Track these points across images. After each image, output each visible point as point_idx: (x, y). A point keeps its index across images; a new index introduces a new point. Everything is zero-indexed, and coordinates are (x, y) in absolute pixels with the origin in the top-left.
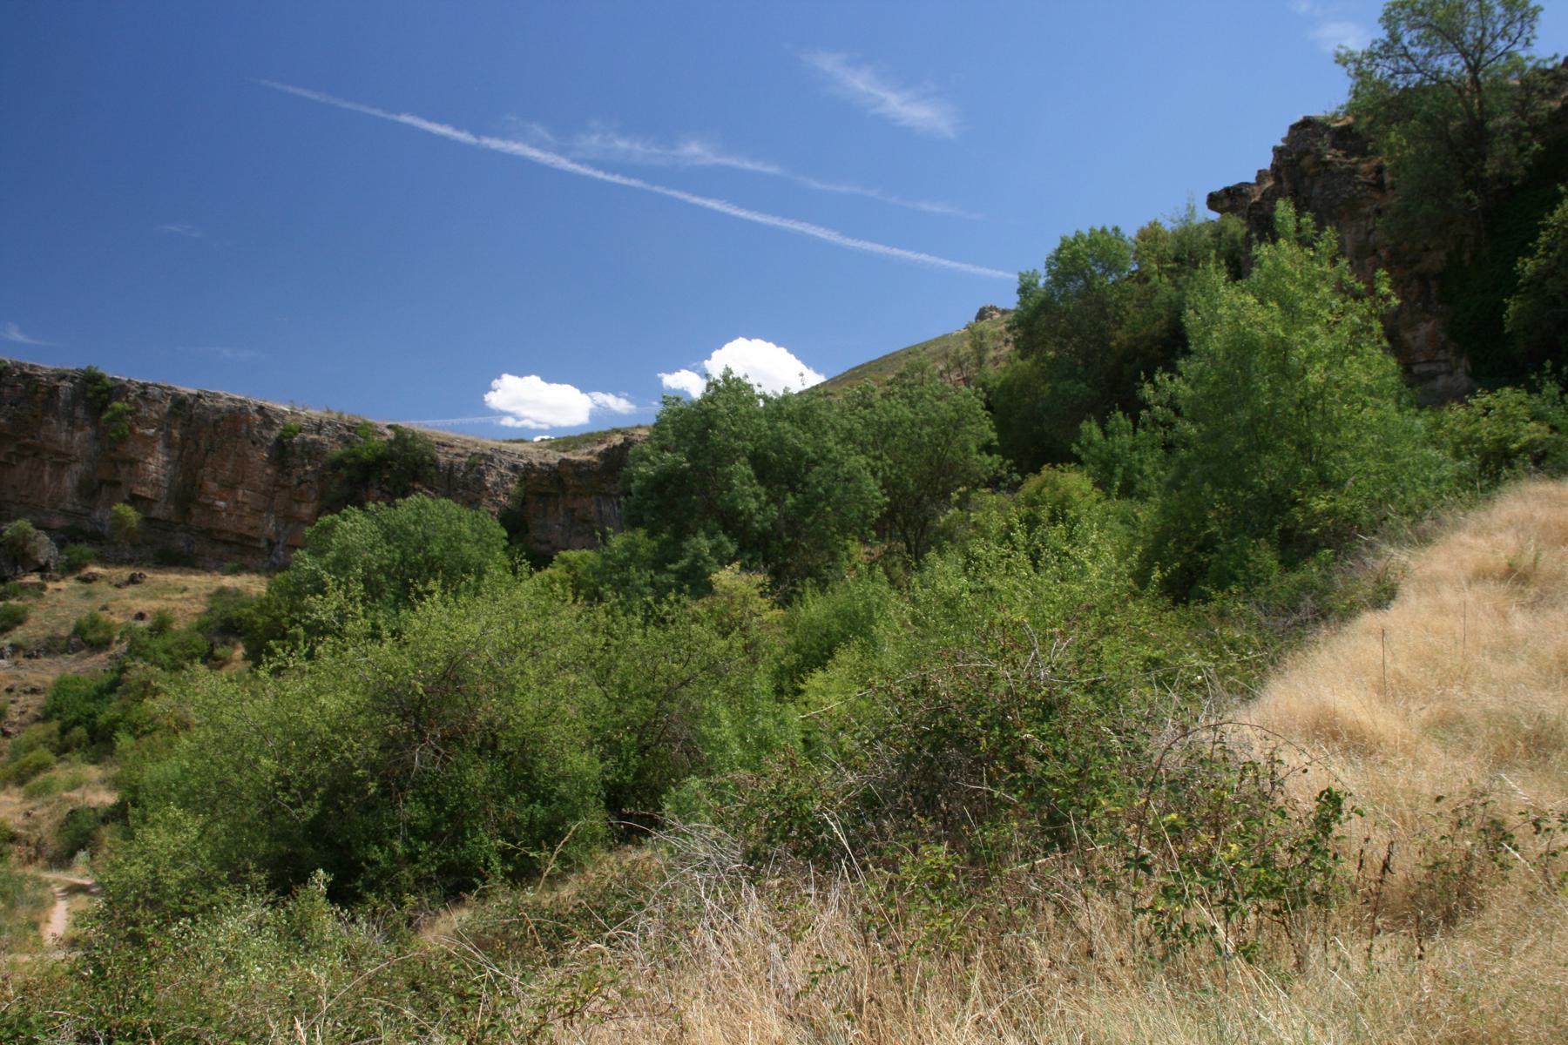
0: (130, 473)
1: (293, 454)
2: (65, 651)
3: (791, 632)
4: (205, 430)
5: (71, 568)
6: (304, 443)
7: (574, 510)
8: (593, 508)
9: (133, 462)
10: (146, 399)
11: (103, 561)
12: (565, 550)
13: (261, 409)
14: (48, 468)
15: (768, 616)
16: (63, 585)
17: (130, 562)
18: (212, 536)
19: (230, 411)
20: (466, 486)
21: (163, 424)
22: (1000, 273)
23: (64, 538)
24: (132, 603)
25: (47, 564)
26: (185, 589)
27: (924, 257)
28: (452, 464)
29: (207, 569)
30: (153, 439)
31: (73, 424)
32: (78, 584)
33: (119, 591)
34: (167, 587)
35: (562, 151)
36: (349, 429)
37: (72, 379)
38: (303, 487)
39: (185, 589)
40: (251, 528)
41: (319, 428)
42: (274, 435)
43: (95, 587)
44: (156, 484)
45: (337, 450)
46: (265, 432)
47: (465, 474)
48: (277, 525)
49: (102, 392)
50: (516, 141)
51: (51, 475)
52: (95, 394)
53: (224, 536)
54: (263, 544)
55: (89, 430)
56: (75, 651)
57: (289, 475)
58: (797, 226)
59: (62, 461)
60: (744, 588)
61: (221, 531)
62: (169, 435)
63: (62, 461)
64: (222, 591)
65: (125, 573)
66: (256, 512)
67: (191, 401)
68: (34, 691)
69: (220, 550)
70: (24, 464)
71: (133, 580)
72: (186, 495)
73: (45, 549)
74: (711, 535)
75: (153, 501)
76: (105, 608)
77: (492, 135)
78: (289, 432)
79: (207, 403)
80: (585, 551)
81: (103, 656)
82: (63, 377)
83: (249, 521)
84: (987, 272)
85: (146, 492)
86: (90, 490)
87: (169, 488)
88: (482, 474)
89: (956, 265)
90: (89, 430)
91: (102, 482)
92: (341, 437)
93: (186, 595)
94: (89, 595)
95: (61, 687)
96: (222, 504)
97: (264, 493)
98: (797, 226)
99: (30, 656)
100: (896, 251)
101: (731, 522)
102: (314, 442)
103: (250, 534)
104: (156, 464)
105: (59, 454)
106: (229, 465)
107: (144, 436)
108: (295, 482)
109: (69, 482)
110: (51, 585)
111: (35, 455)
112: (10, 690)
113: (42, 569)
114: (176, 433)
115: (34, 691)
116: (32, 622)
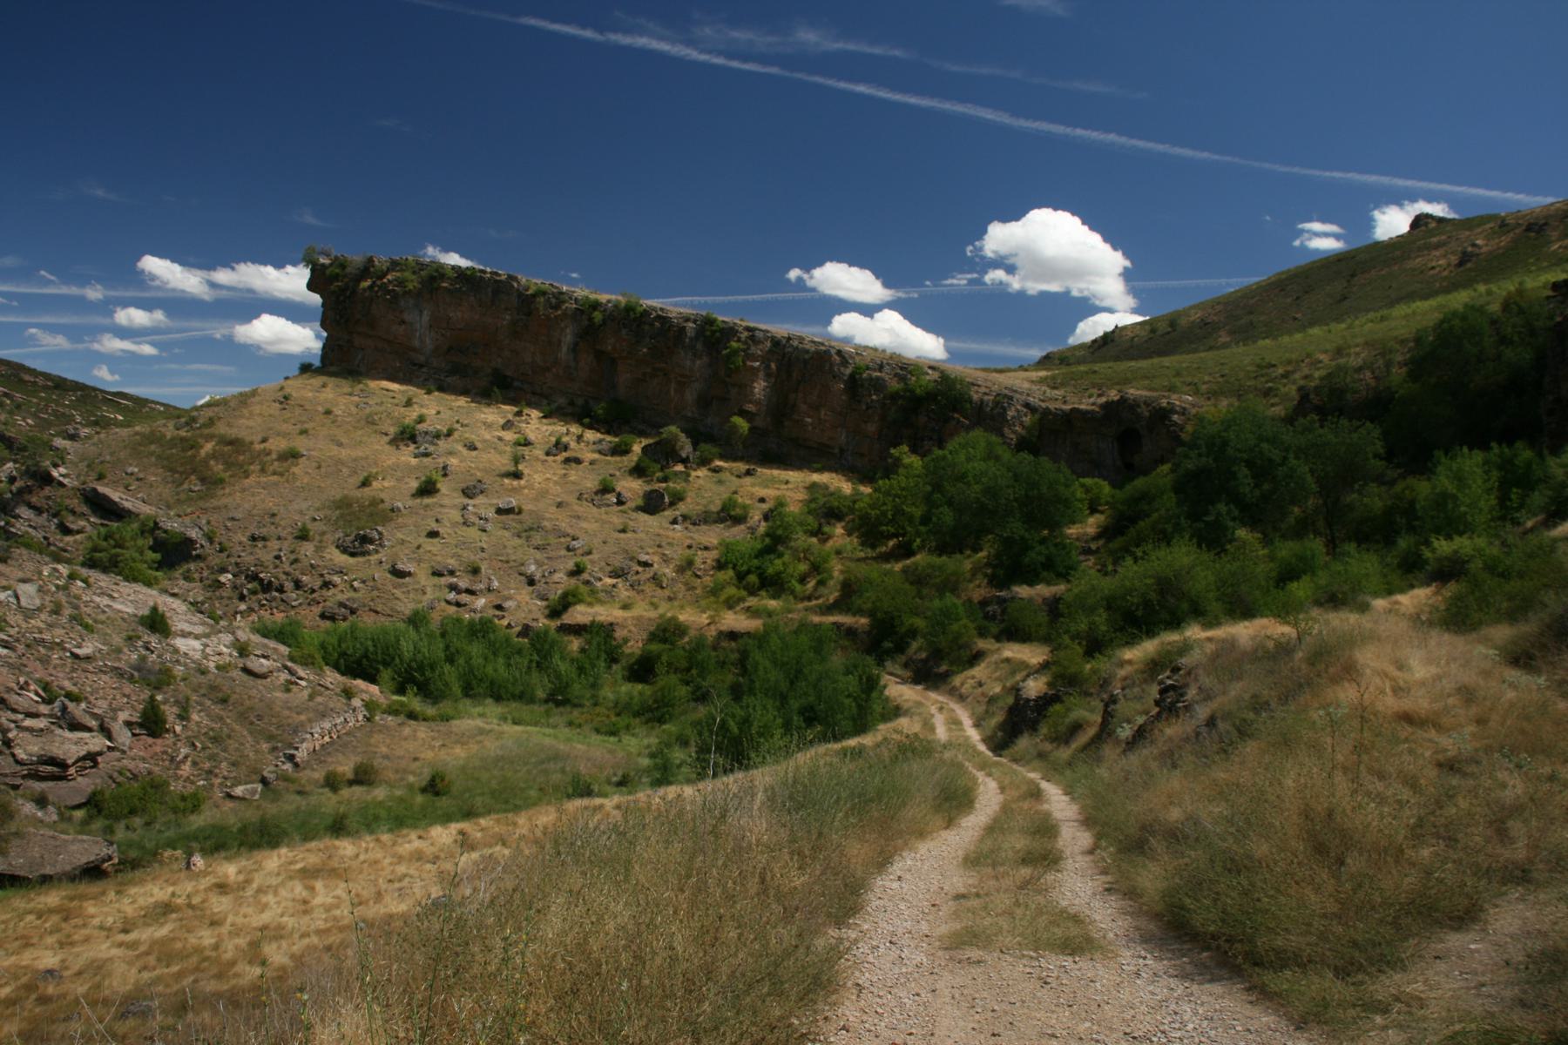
5: (704, 462)
6: (871, 379)
11: (723, 457)
14: (673, 385)
16: (699, 473)
17: (748, 462)
19: (817, 353)
21: (765, 360)
22: (1205, 155)
23: (697, 438)
26: (787, 482)
27: (1112, 137)
29: (799, 468)
30: (757, 369)
34: (773, 480)
35: (689, 43)
37: (695, 321)
39: (787, 482)
42: (848, 371)
44: (758, 403)
45: (894, 385)
50: (641, 35)
52: (713, 336)
58: (959, 108)
62: (768, 367)
64: (813, 487)
65: (742, 467)
68: (706, 548)
71: (748, 473)
72: (780, 409)
73: (686, 449)
77: (615, 31)
79: (795, 343)
82: (687, 320)
84: (1188, 152)
85: (751, 408)
88: (1004, 409)
89: (1150, 145)
90: (706, 359)
92: (896, 375)
94: (720, 482)
95: (727, 547)
98: (959, 108)
99: (694, 524)
100: (1079, 132)
102: (878, 378)
104: (759, 387)
107: (752, 368)
109: (690, 396)
110: (694, 474)
112: (690, 547)
113: (685, 461)
114: (773, 366)
115: (706, 548)
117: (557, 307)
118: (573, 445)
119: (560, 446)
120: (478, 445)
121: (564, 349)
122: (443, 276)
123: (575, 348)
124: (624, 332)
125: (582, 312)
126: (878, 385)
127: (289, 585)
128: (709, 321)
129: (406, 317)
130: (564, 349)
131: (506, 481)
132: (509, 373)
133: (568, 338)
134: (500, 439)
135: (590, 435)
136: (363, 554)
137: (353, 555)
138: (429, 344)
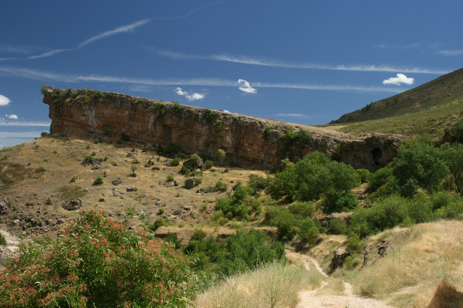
0: (221, 140)
1: (269, 135)
2: (214, 191)
3: (432, 200)
4: (241, 128)
5: (208, 167)
6: (272, 132)
7: (356, 155)
8: (362, 155)
9: (222, 137)
10: (226, 119)
11: (215, 165)
12: (359, 169)
13: (260, 122)
14: (194, 137)
15: (427, 197)
18: (244, 158)
20: (321, 146)
23: (205, 159)
24: (228, 178)
25: (202, 166)
26: (241, 174)
28: (317, 140)
30: (228, 130)
31: (203, 125)
32: (210, 172)
33: (223, 174)
36: (285, 128)
37: (202, 112)
38: (273, 145)
40: (257, 157)
41: (276, 128)
42: (264, 130)
43: (215, 173)
45: (282, 135)
46: (261, 129)
47: (321, 143)
48: (264, 156)
49: (211, 116)
51: (195, 140)
52: (209, 117)
53: (249, 159)
54: (260, 161)
55: (207, 127)
56: (216, 191)
57: (268, 142)
59: (199, 136)
60: (423, 193)
61: (247, 157)
63: (199, 136)
64: (252, 176)
65: (223, 169)
66: (259, 152)
67: (238, 119)
68: (211, 202)
69: (247, 162)
70: (187, 136)
71: (226, 171)
72: (238, 147)
73: (200, 162)
74: (413, 179)
75: (227, 148)
76: (221, 179)
78: (267, 130)
79: (242, 119)
80: (364, 169)
81: (225, 193)
82: (199, 112)
83: (257, 155)
86: (207, 144)
87: (232, 144)
88: (326, 142)
90: (207, 127)
91: (210, 142)
92: (283, 130)
93: (242, 176)
96: (249, 150)
97: (261, 147)
99: (206, 192)
101: (417, 177)
102: (275, 132)
103: (257, 158)
105: (198, 134)
106: (251, 139)
108: (270, 144)
109: (201, 142)
110: (204, 172)
111: (191, 133)
112: (204, 202)
113: (200, 168)
115: (211, 202)
116: (203, 183)
117: (146, 108)
118: (155, 162)
119: (150, 163)
120: (118, 164)
121: (150, 124)
122: (100, 96)
123: (155, 124)
124: (174, 117)
125: (157, 109)
126: (276, 135)
127: (43, 223)
128: (207, 112)
129: (86, 113)
130: (150, 124)
131: (130, 178)
132: (128, 134)
133: (152, 120)
134: (126, 161)
135: (162, 158)
136: (73, 209)
137: (69, 210)
138: (95, 125)
